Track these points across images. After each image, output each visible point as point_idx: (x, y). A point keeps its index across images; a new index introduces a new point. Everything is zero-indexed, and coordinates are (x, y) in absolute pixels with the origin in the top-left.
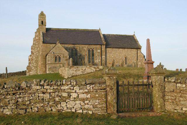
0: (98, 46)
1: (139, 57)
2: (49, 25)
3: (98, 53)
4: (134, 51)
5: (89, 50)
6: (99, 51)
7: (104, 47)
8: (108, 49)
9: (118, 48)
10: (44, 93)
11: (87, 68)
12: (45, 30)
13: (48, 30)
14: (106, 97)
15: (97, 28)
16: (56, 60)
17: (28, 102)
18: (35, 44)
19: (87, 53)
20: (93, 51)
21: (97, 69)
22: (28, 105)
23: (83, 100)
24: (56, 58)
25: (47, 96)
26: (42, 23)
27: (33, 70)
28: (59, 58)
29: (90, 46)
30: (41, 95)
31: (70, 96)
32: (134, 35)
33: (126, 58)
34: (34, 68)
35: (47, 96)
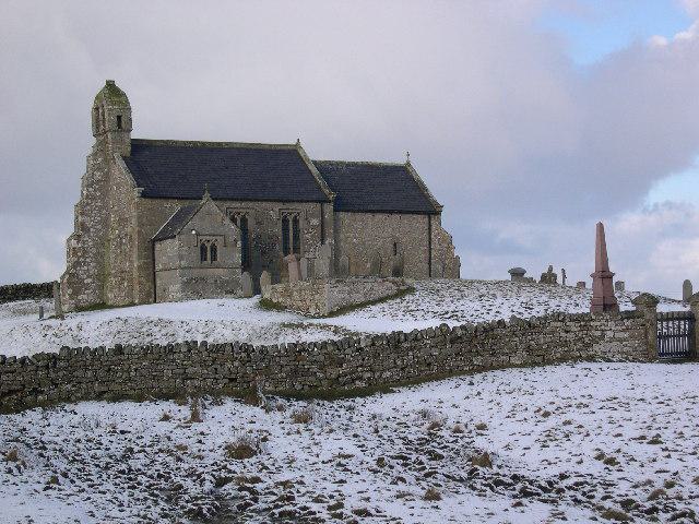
0: (312, 205)
1: (435, 240)
2: (146, 126)
3: (314, 227)
4: (420, 221)
5: (285, 221)
6: (315, 222)
7: (329, 208)
8: (342, 215)
9: (370, 211)
10: (567, 332)
11: (376, 284)
12: (129, 149)
13: (138, 146)
14: (646, 337)
15: (400, 161)
16: (203, 258)
17: (598, 333)
18: (94, 198)
19: (278, 230)
20: (296, 221)
21: (402, 288)
22: (546, 350)
23: (621, 340)
24: (203, 249)
25: (571, 336)
26: (122, 122)
27: (87, 287)
28: (214, 249)
29: (288, 205)
30: (563, 334)
31: (603, 336)
32: (408, 164)
33: (395, 245)
34: (89, 280)
35: (571, 336)
